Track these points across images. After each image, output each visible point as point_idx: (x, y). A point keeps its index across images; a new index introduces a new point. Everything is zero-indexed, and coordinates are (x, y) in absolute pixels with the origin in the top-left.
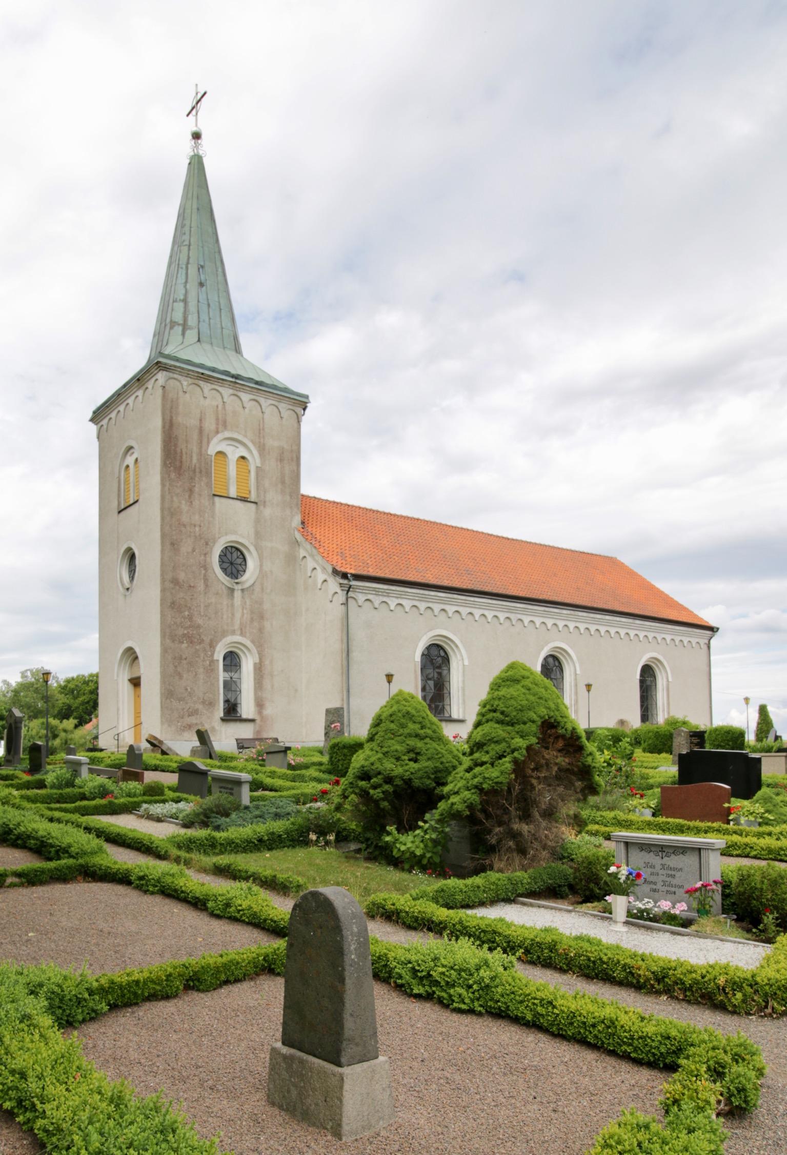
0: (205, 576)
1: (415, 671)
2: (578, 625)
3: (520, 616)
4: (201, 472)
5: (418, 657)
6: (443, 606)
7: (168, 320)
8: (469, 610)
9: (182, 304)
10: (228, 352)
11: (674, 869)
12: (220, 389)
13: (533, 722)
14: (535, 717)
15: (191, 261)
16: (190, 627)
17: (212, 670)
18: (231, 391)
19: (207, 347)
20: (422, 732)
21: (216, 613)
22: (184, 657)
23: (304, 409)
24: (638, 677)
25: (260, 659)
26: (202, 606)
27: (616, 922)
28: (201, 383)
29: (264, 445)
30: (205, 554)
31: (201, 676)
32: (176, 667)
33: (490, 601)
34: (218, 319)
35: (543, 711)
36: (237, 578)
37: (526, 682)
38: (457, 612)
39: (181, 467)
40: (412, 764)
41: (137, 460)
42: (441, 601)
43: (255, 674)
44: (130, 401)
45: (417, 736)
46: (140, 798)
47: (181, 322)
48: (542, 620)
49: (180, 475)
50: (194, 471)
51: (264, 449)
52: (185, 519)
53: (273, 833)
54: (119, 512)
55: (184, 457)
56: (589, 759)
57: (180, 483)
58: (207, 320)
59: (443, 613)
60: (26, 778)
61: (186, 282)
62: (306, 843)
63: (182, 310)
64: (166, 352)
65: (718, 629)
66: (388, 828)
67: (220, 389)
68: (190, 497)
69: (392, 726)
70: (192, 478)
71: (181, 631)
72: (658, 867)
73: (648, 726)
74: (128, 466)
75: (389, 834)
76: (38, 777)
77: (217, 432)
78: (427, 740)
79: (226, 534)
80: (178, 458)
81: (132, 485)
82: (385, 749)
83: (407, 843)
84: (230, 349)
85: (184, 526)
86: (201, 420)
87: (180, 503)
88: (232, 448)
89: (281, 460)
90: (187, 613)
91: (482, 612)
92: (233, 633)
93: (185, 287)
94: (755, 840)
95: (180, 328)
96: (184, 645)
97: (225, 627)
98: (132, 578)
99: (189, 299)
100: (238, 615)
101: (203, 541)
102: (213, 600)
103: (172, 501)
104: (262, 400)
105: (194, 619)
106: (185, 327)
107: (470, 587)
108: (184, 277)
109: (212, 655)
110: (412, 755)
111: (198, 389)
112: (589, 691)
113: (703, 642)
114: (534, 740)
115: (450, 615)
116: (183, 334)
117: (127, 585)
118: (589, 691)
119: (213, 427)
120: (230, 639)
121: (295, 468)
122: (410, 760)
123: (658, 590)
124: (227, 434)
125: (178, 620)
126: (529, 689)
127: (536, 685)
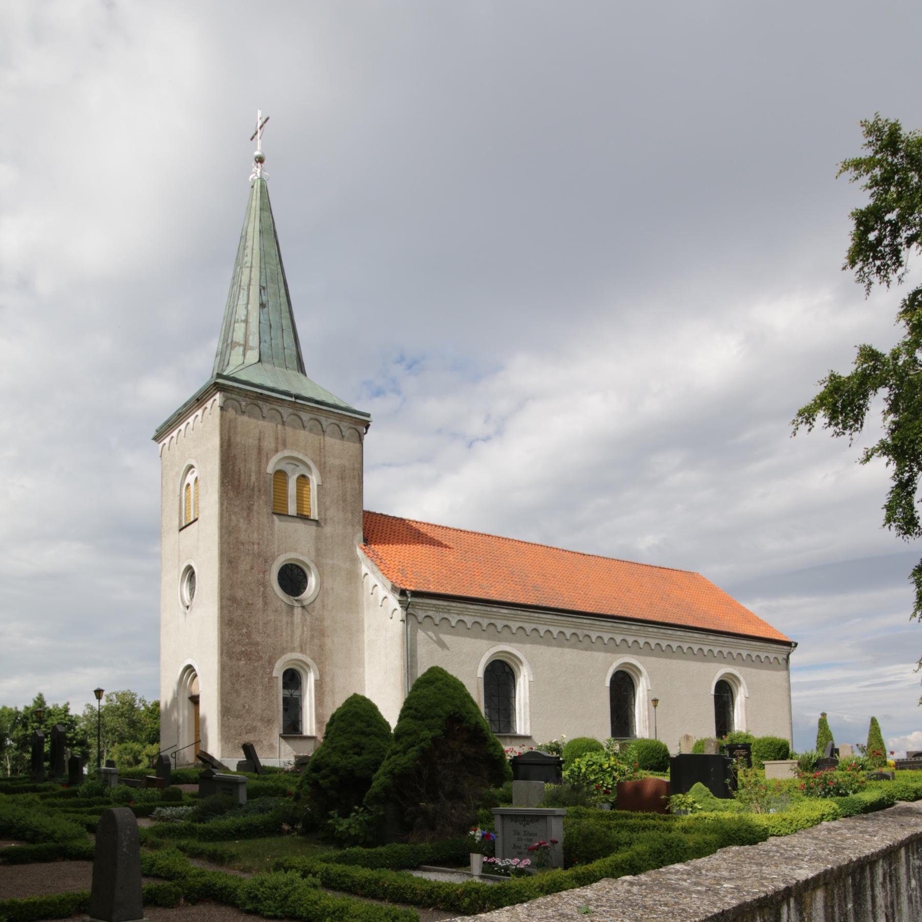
0: (264, 593)
1: (478, 687)
2: (648, 640)
3: (587, 632)
4: (259, 491)
5: (608, 684)
6: (506, 623)
7: (229, 341)
8: (534, 626)
9: (243, 325)
10: (290, 372)
11: (531, 834)
12: (279, 409)
13: (440, 717)
14: (441, 712)
15: (253, 282)
16: (247, 644)
17: (271, 687)
18: (290, 411)
19: (268, 366)
20: (368, 730)
21: (275, 630)
22: (242, 674)
23: (367, 428)
24: (713, 692)
25: (321, 676)
26: (261, 623)
27: (473, 876)
28: (260, 403)
29: (325, 463)
30: (264, 572)
31: (260, 694)
32: (233, 684)
33: (555, 617)
34: (280, 340)
35: (449, 707)
36: (298, 595)
37: (439, 684)
38: (521, 628)
39: (239, 486)
40: (356, 758)
41: (196, 479)
42: (504, 617)
43: (316, 691)
44: (191, 420)
45: (363, 733)
46: (157, 803)
47: (242, 342)
48: (610, 636)
49: (238, 493)
50: (253, 490)
51: (325, 468)
52: (243, 537)
53: (251, 825)
54: (180, 530)
55: (243, 476)
56: (492, 749)
57: (238, 502)
58: (268, 339)
59: (506, 629)
60: (61, 789)
61: (248, 303)
62: (281, 833)
63: (243, 330)
64: (225, 374)
65: (796, 644)
66: (331, 812)
67: (279, 409)
68: (248, 516)
69: (342, 724)
70: (251, 497)
71: (238, 649)
72: (522, 833)
73: (726, 741)
74: (188, 485)
75: (332, 818)
76: (73, 788)
77: (277, 451)
78: (372, 736)
79: (286, 552)
80: (236, 477)
81: (192, 503)
82: (334, 745)
83: (343, 825)
84: (293, 369)
85: (243, 544)
86: (259, 439)
87: (238, 521)
88: (292, 467)
89: (343, 478)
90: (245, 630)
91: (547, 628)
92: (293, 650)
93: (247, 308)
94: (662, 822)
95: (241, 349)
96: (242, 663)
97: (285, 645)
98: (192, 594)
99: (250, 320)
100: (298, 633)
101: (261, 559)
102: (272, 618)
103: (230, 520)
104: (323, 419)
105: (253, 636)
106: (246, 347)
107: (535, 603)
108: (245, 298)
109: (271, 672)
110: (356, 750)
111: (257, 409)
112: (655, 706)
113: (781, 657)
114: (439, 732)
115: (514, 631)
116: (244, 355)
117: (188, 603)
118: (655, 706)
119: (273, 446)
120: (290, 656)
121: (357, 486)
122: (354, 754)
123: (747, 611)
124: (287, 453)
125: (236, 638)
126: (440, 690)
127: (447, 686)
